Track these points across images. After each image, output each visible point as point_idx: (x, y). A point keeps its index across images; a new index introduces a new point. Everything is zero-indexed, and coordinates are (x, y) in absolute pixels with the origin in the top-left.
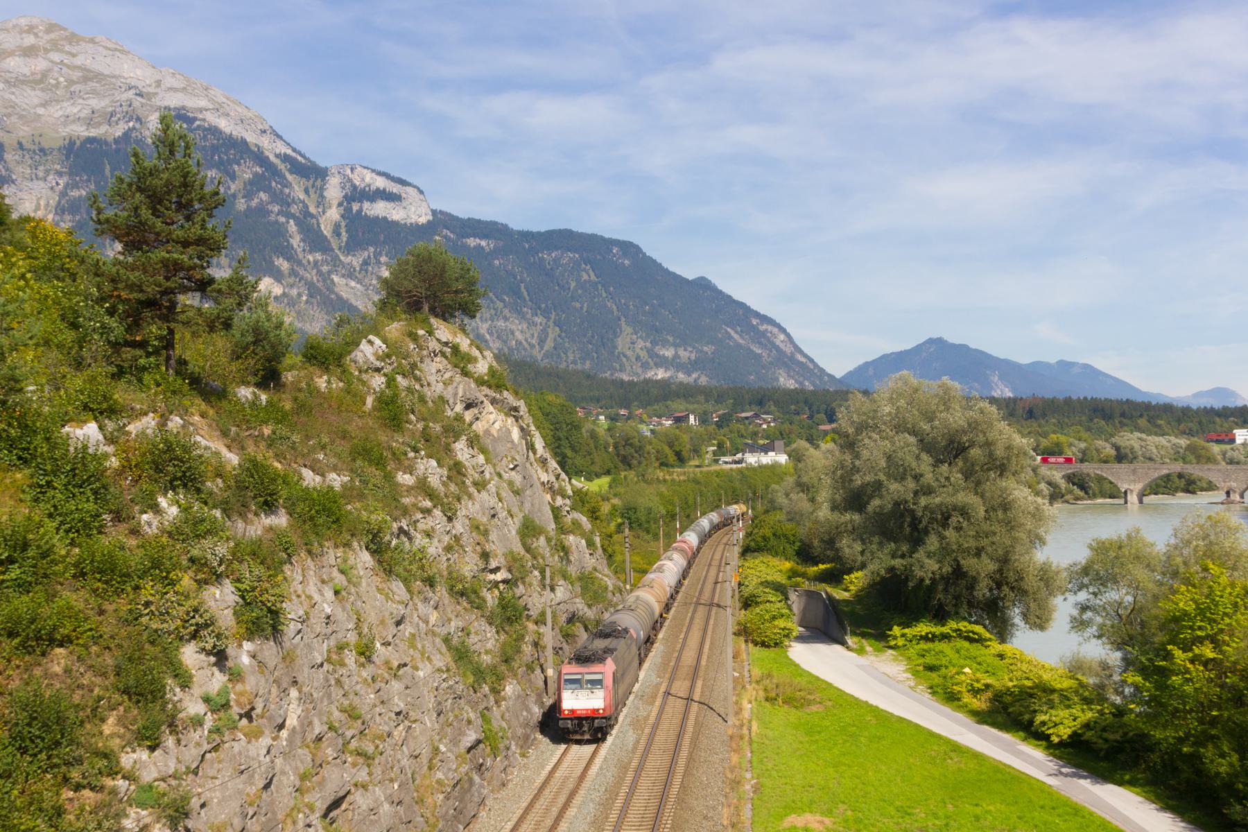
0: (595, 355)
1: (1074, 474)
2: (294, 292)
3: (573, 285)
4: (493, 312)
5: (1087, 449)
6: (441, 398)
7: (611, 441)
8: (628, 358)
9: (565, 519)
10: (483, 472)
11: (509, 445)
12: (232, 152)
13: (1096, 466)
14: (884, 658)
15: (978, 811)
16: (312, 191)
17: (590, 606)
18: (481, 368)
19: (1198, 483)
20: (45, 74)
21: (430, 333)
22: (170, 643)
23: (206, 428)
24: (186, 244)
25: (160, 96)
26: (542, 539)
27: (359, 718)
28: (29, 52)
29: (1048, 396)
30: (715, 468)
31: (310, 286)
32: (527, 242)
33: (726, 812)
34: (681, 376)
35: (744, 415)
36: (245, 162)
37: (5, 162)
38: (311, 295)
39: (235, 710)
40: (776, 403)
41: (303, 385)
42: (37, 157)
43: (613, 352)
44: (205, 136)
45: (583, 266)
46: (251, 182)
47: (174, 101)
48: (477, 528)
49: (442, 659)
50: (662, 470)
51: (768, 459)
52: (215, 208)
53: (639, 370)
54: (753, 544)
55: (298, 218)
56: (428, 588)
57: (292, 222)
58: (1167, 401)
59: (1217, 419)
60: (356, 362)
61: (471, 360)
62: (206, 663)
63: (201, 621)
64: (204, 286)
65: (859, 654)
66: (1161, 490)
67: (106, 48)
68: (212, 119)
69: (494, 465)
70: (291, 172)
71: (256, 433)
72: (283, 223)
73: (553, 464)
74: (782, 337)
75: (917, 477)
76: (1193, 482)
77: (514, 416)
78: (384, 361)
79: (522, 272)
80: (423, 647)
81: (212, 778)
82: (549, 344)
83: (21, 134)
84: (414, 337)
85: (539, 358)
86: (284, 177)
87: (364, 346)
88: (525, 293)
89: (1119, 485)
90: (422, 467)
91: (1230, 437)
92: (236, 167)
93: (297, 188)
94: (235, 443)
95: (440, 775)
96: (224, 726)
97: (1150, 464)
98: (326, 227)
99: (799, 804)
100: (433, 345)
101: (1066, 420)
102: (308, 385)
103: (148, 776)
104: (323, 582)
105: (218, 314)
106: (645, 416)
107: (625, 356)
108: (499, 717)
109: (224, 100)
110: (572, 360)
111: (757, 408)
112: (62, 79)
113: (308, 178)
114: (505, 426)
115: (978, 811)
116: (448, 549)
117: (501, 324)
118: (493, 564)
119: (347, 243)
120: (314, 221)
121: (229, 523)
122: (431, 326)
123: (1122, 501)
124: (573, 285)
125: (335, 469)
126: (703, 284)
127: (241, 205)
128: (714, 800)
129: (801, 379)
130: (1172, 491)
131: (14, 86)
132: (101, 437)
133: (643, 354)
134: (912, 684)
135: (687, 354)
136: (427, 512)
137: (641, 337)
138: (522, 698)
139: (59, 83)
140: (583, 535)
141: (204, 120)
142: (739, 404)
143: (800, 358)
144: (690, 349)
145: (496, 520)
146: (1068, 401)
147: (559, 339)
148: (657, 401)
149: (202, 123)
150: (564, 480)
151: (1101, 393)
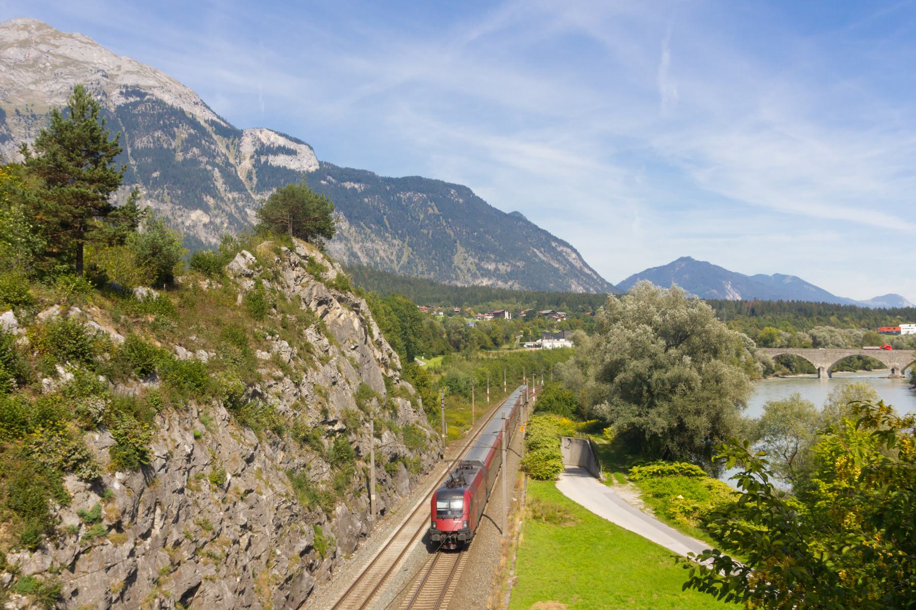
0: (438, 268)
1: (781, 356)
2: (218, 221)
3: (422, 216)
4: (363, 236)
5: (791, 338)
6: (299, 297)
7: (444, 330)
8: (462, 271)
9: (395, 386)
10: (327, 351)
11: (351, 332)
12: (173, 118)
13: (797, 350)
14: (625, 488)
15: (675, 598)
16: (231, 147)
17: (411, 450)
18: (332, 275)
19: (872, 363)
20: (36, 60)
21: (292, 249)
22: (54, 473)
23: (100, 316)
24: (92, 181)
25: (120, 77)
26: (374, 400)
27: (210, 529)
28: (24, 44)
29: (767, 299)
30: (521, 350)
31: (230, 216)
32: (389, 185)
33: (490, 599)
34: (500, 284)
35: (544, 312)
36: (183, 126)
37: (6, 124)
38: (230, 223)
39: (106, 523)
40: (570, 305)
41: (191, 286)
42: (30, 121)
43: (450, 266)
44: (153, 107)
45: (429, 203)
46: (187, 141)
47: (130, 81)
48: (320, 391)
49: (283, 487)
50: (482, 352)
51: (559, 344)
52: (115, 155)
53: (470, 279)
54: (541, 405)
55: (221, 166)
56: (276, 435)
57: (216, 169)
58: (853, 303)
59: (888, 317)
60: (232, 270)
61: (324, 269)
62: (83, 488)
63: (80, 457)
64: (105, 211)
65: (607, 485)
66: (845, 368)
67: (81, 42)
68: (159, 94)
69: (339, 346)
70: (216, 134)
71: (143, 320)
72: (210, 171)
73: (387, 346)
74: (574, 255)
75: (652, 356)
76: (869, 362)
77: (355, 311)
78: (254, 269)
79: (384, 208)
80: (268, 478)
81: (83, 572)
82: (405, 259)
83: (18, 104)
84: (278, 252)
85: (397, 270)
86: (211, 137)
87: (238, 258)
88: (387, 223)
89: (814, 364)
90: (277, 347)
91: (897, 329)
92: (175, 129)
93: (221, 145)
94: (123, 327)
95: (275, 572)
96: (95, 535)
97: (838, 350)
98: (241, 173)
99: (545, 594)
100: (294, 258)
101: (778, 317)
102: (194, 286)
103: (27, 571)
104: (186, 429)
105: (115, 233)
106: (472, 313)
107: (459, 269)
108: (330, 530)
109: (168, 80)
110: (421, 271)
111: (554, 307)
112: (48, 64)
113: (229, 138)
114: (348, 318)
115: (675, 598)
116: (295, 407)
117: (369, 245)
118: (331, 418)
119: (257, 185)
120: (233, 169)
121: (111, 385)
122: (292, 244)
123: (816, 376)
124: (422, 216)
125: (204, 347)
126: (516, 217)
127: (179, 157)
128: (482, 591)
129: (587, 286)
130: (854, 369)
131: (13, 69)
132: (15, 322)
133: (473, 268)
134: (642, 507)
135: (504, 267)
136: (279, 379)
137: (471, 255)
138: (348, 516)
139: (46, 67)
140: (409, 397)
141: (153, 95)
142: (541, 304)
143: (586, 270)
144: (507, 264)
145: (336, 386)
146: (780, 303)
147: (411, 256)
148: (482, 301)
149: (151, 97)
150: (395, 358)
151: (805, 298)
